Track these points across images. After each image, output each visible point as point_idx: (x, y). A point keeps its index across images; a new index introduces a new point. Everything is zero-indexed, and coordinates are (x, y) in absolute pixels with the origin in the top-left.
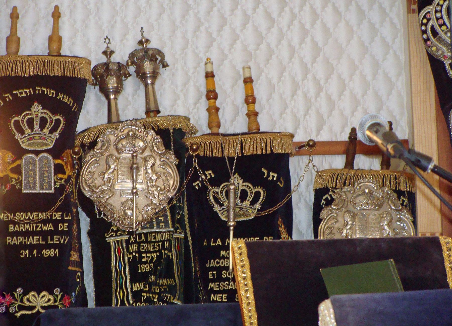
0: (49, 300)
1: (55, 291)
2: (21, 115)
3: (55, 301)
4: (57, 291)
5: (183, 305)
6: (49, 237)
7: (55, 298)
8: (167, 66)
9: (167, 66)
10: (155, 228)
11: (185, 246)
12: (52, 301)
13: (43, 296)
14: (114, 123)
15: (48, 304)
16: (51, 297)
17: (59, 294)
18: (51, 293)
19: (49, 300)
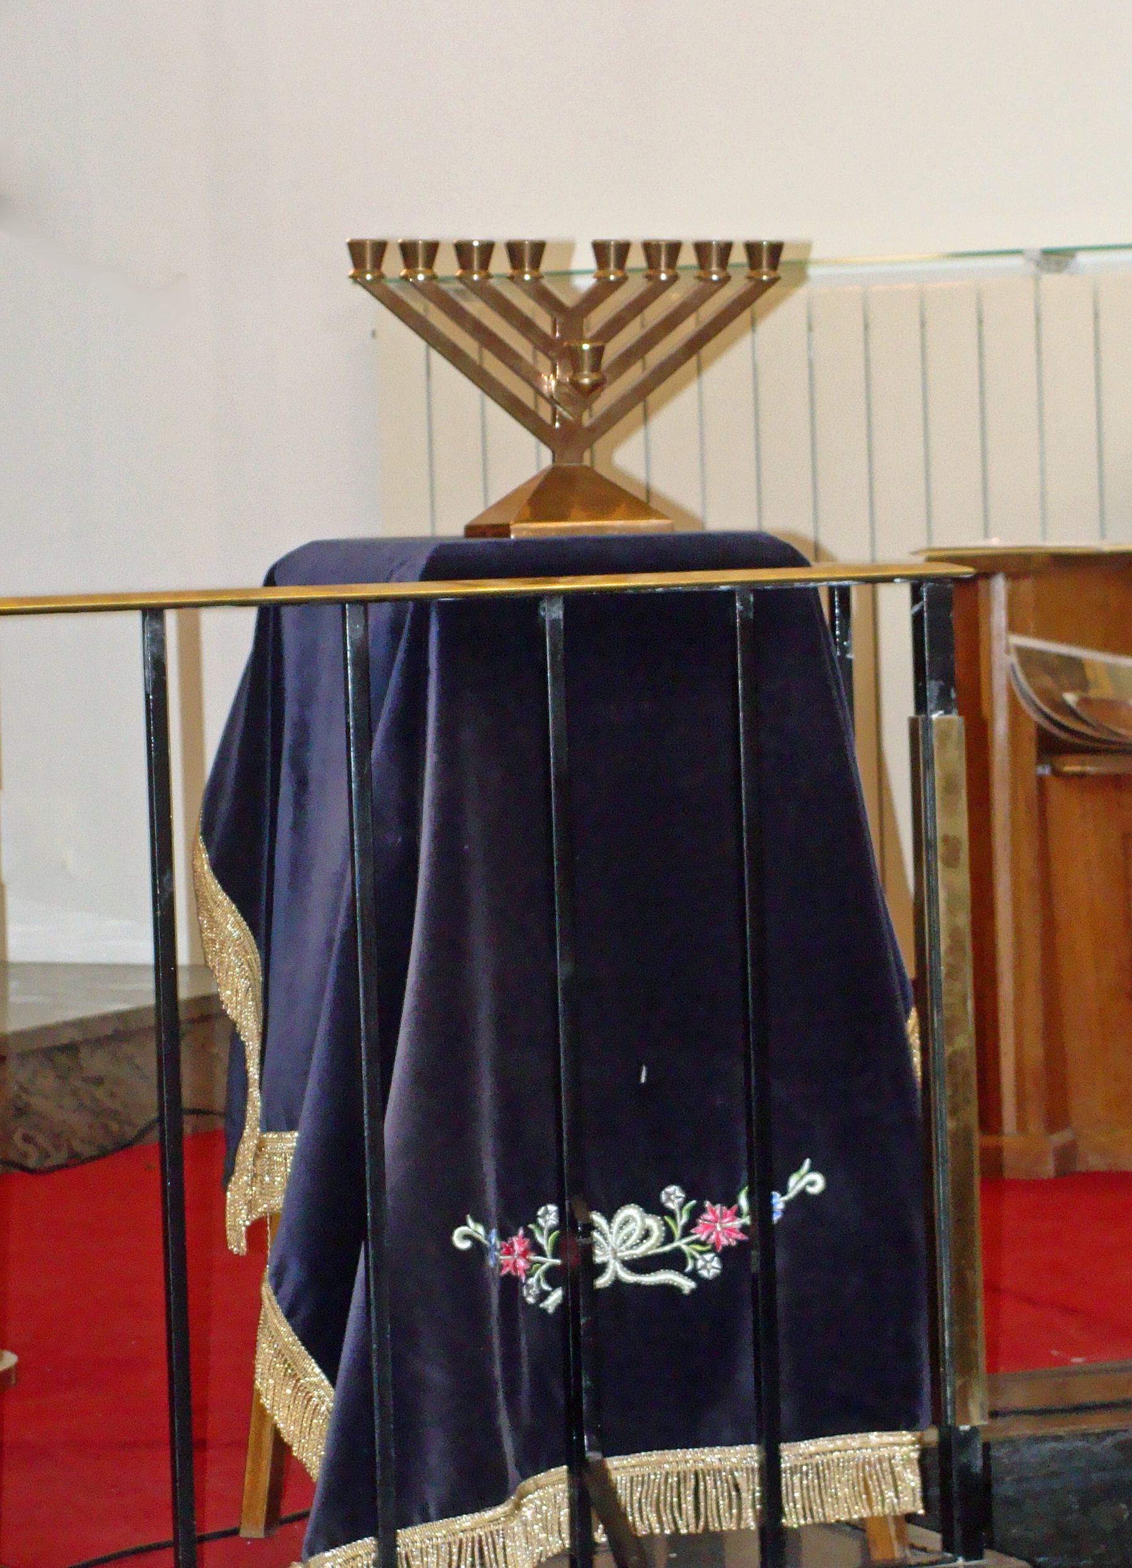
0: (647, 1235)
1: (663, 1197)
2: (563, 982)
3: (669, 1237)
4: (673, 1196)
5: (910, 983)
6: (643, 1080)
7: (666, 1224)
8: (356, 248)
9: (356, 248)
10: (554, 612)
11: (400, 639)
12: (657, 1233)
13: (626, 1222)
14: (1007, 639)
15: (639, 1252)
16: (654, 1223)
17: (681, 1208)
18: (654, 1207)
19: (647, 1235)
